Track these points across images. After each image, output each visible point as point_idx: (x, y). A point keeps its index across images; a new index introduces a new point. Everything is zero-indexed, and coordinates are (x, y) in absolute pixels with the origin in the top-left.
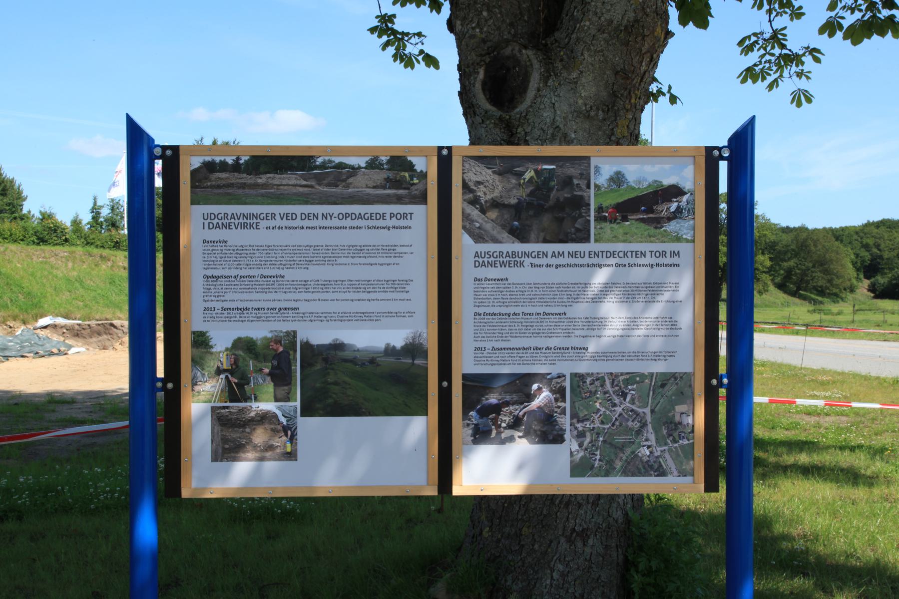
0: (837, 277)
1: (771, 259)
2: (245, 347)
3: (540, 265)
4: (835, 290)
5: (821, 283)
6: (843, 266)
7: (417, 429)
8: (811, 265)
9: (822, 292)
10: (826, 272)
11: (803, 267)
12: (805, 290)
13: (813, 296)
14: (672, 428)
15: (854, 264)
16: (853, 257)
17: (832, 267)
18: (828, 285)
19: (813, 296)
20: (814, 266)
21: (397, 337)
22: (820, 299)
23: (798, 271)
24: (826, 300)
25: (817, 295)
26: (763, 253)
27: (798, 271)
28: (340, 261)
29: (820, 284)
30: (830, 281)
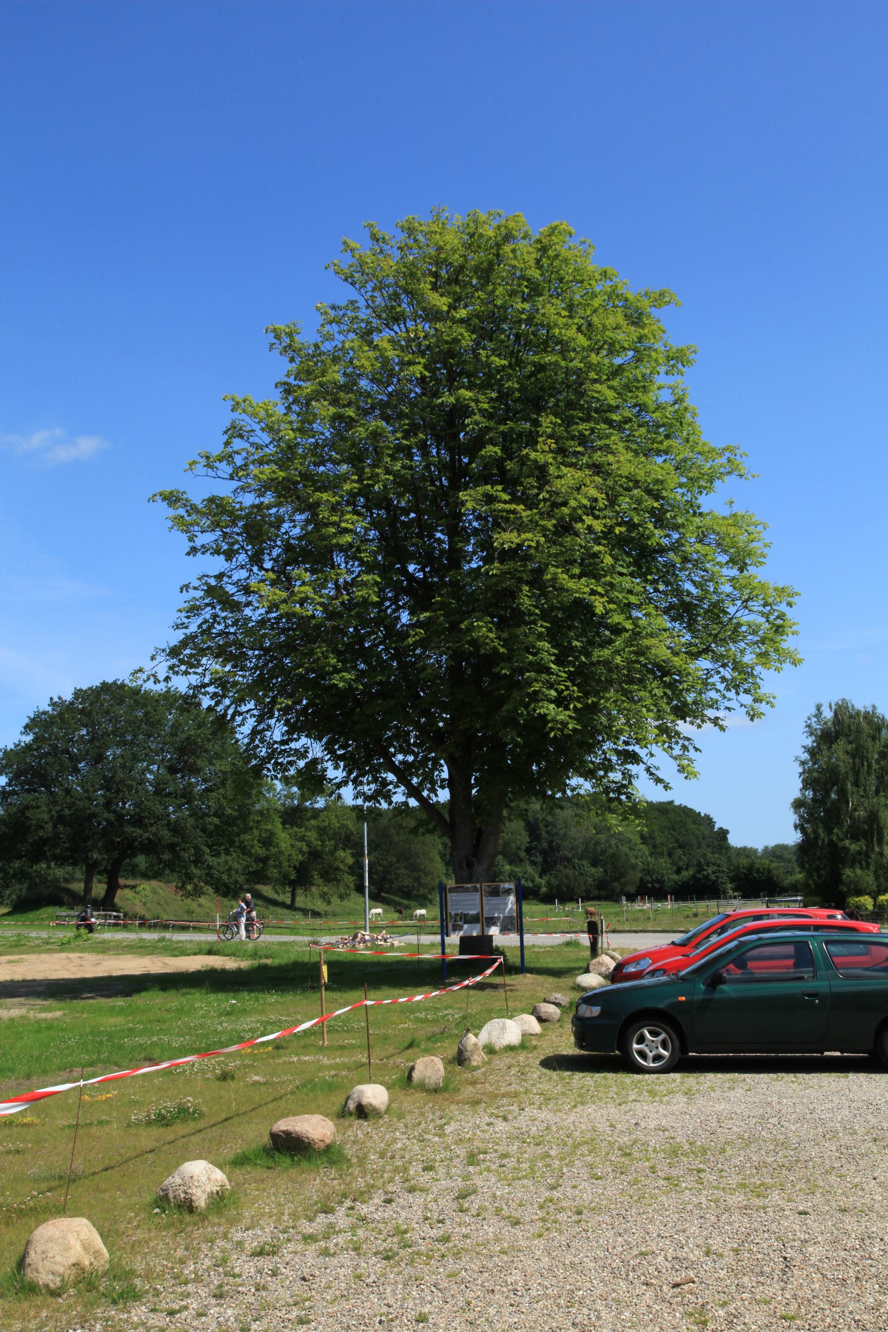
0: (426, 875)
1: (353, 855)
2: (456, 915)
3: (494, 900)
4: (423, 891)
5: (407, 882)
6: (431, 860)
7: (479, 926)
8: (394, 860)
9: (407, 894)
10: (413, 868)
11: (386, 863)
12: (388, 892)
13: (397, 899)
14: (512, 924)
15: (442, 856)
16: (440, 847)
17: (418, 861)
18: (416, 884)
19: (397, 899)
20: (398, 862)
21: (475, 912)
22: (405, 902)
23: (379, 868)
24: (412, 903)
25: (401, 897)
26: (344, 850)
27: (379, 868)
28: (267, 890)
29: (406, 883)
30: (417, 880)
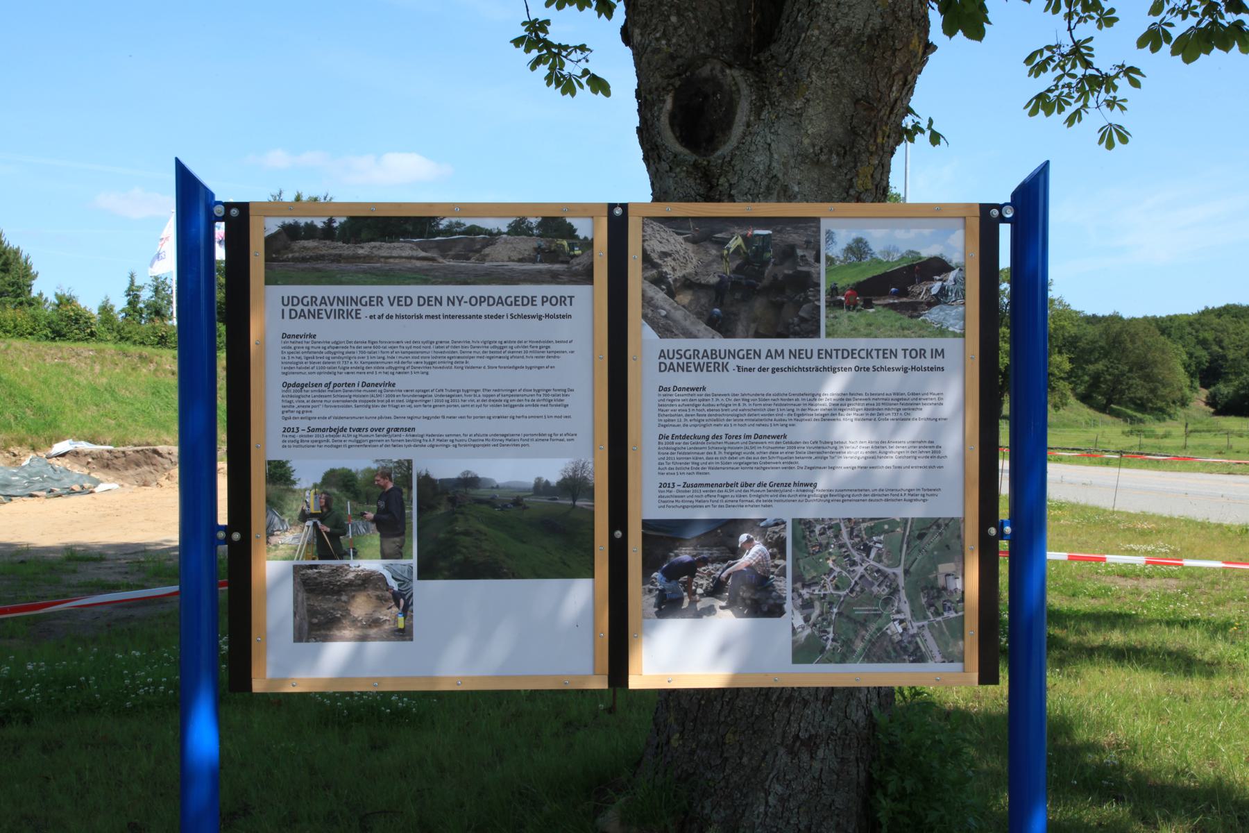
0: (1163, 385)
1: (1071, 360)
2: (340, 482)
3: (750, 369)
4: (1160, 404)
5: (1141, 393)
6: (1171, 370)
7: (580, 597)
8: (1126, 368)
9: (1141, 406)
10: (1148, 378)
11: (1116, 372)
12: (1119, 404)
13: (1129, 412)
14: (933, 596)
15: (1186, 367)
16: (1185, 357)
17: (1155, 371)
18: (1151, 396)
19: (1129, 412)
20: (1131, 370)
21: (551, 468)
22: (1139, 415)
23: (1108, 377)
24: (1147, 417)
25: (1136, 410)
26: (1060, 352)
27: (1108, 377)
28: (472, 362)
29: (1139, 394)
30: (1153, 391)
